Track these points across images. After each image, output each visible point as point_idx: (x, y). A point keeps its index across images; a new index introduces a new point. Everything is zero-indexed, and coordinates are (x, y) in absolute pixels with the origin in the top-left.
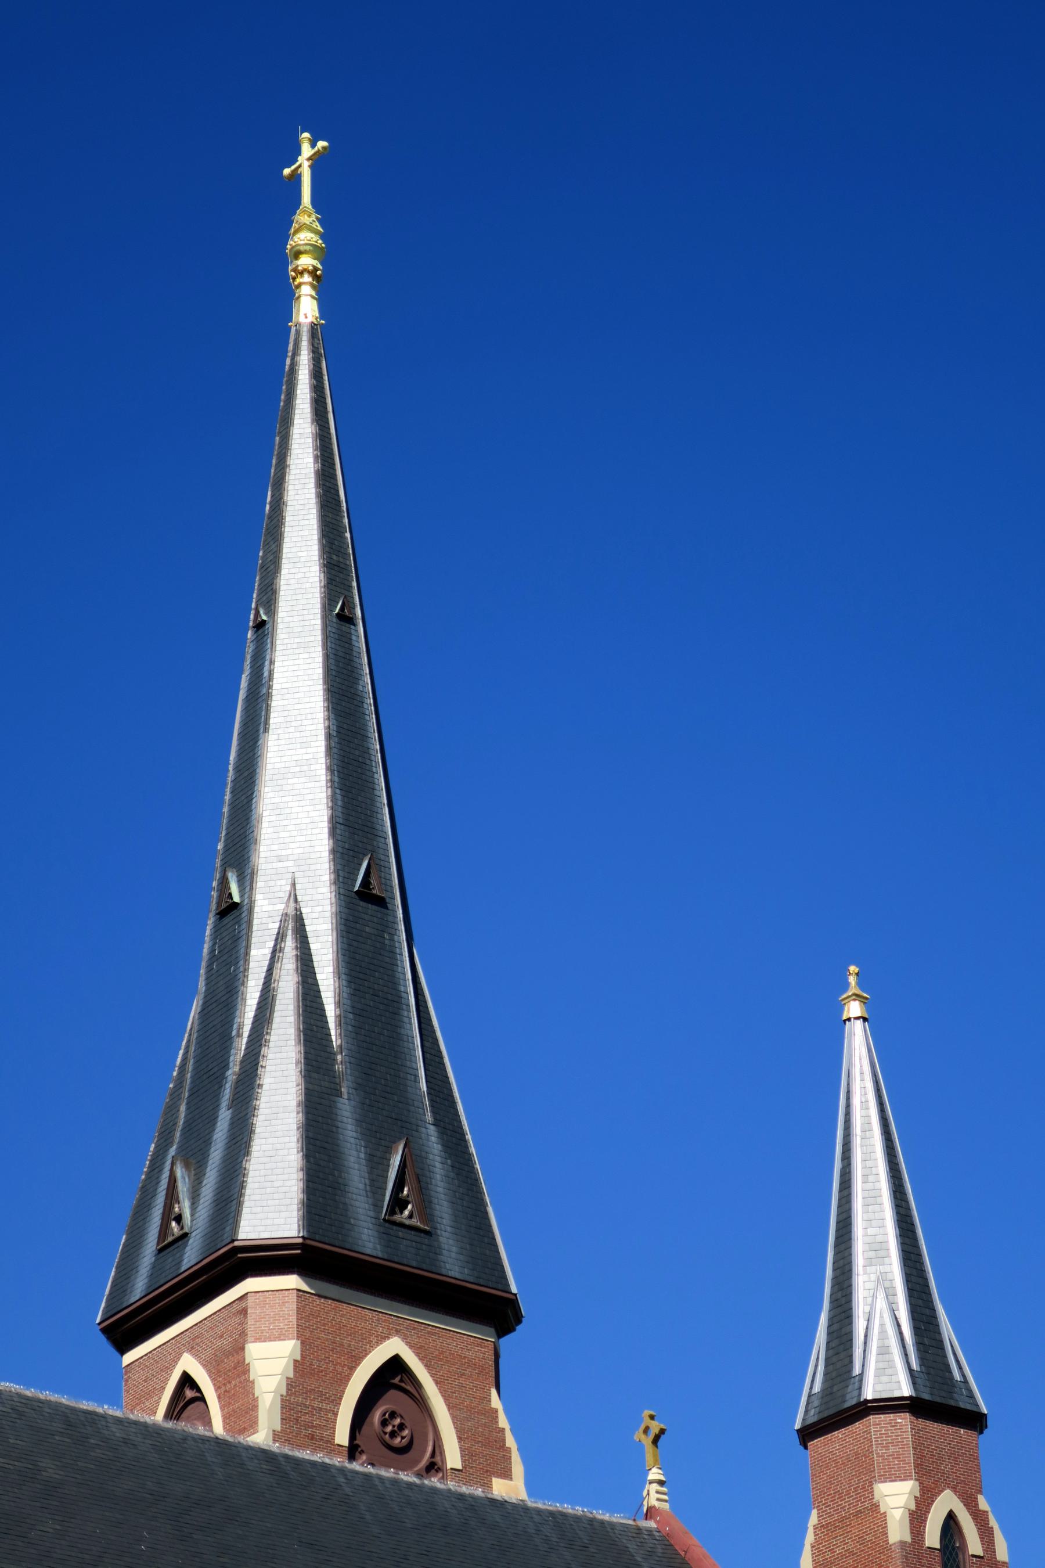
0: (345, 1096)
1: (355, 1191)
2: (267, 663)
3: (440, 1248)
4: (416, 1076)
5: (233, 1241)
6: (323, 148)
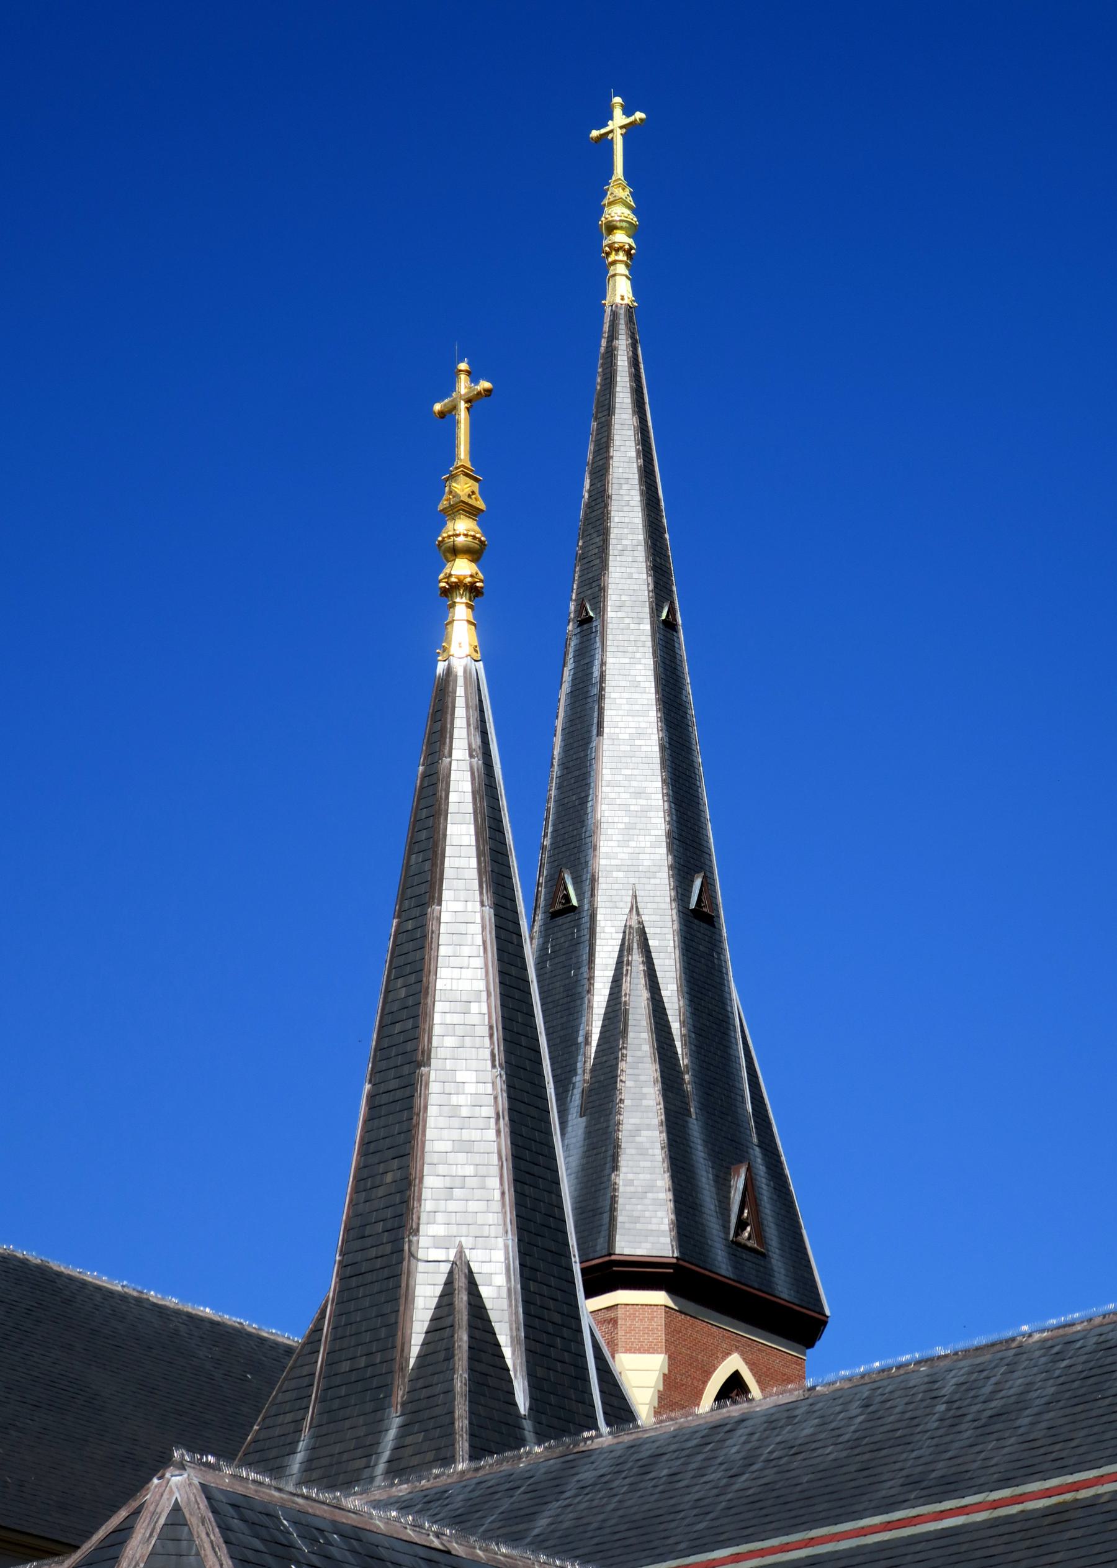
0: (694, 1116)
1: (709, 1212)
2: (597, 663)
3: (772, 1270)
4: (743, 1097)
5: (610, 1255)
6: (641, 119)
